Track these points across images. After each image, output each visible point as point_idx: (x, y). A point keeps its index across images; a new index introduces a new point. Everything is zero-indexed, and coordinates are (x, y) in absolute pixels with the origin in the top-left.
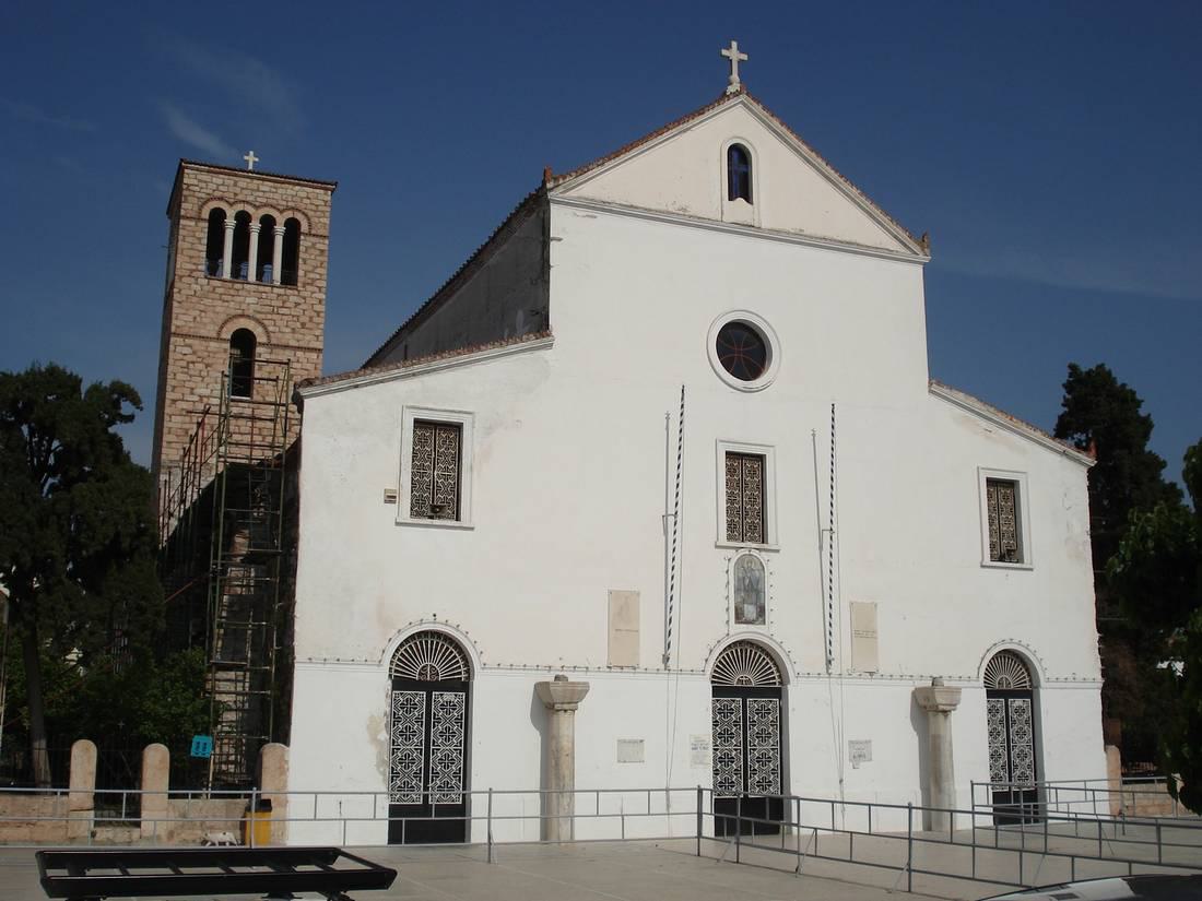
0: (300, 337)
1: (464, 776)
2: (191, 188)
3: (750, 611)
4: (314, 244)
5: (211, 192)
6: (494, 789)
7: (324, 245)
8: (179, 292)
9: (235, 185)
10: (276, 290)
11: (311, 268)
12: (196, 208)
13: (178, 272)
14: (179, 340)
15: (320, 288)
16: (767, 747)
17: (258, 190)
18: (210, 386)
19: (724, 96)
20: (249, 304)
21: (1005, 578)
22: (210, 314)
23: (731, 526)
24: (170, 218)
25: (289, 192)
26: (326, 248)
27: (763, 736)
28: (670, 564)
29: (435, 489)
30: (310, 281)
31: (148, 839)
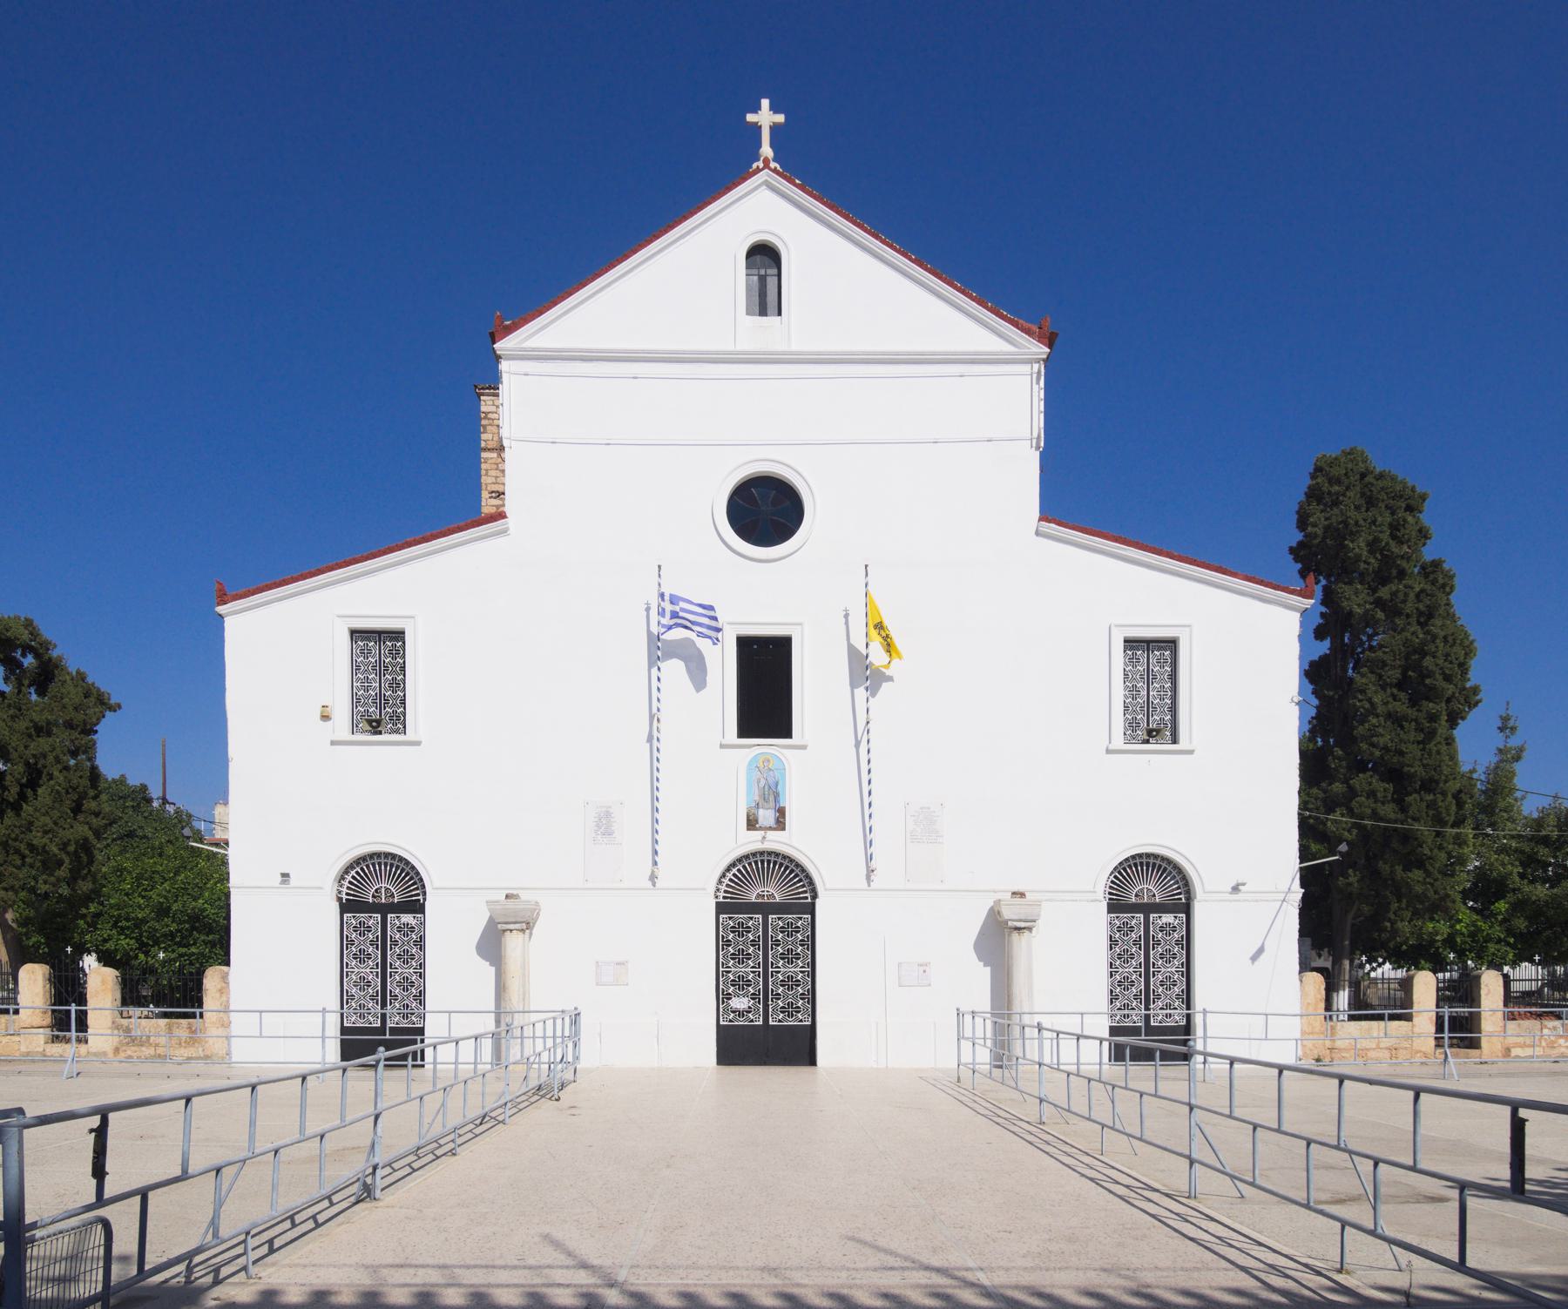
1: (1187, 999)
2: (490, 416)
3: (766, 816)
6: (327, 1009)
16: (795, 970)
23: (1132, 725)
27: (1168, 957)
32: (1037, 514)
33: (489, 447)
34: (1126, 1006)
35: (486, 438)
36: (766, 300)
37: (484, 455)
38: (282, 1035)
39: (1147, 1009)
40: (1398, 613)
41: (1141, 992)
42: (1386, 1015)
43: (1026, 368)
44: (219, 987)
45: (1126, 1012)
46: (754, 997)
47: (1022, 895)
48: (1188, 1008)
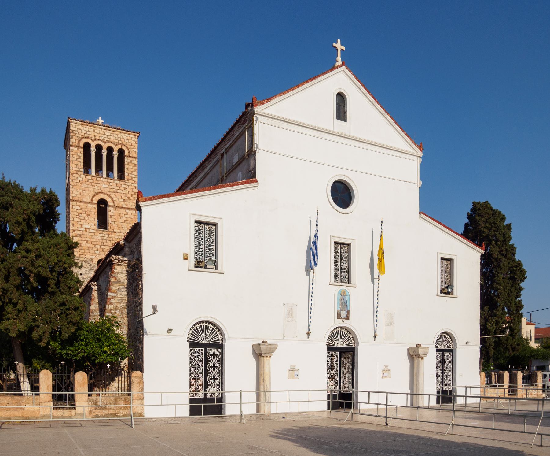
0: (128, 203)
2: (74, 132)
3: (343, 314)
4: (131, 161)
5: (83, 134)
7: (136, 161)
8: (72, 181)
9: (94, 131)
10: (115, 182)
11: (131, 172)
12: (77, 142)
13: (71, 172)
14: (74, 203)
15: (135, 181)
17: (105, 134)
18: (89, 224)
19: (333, 68)
20: (104, 188)
21: (446, 300)
22: (87, 192)
23: (336, 276)
24: (65, 149)
25: (119, 136)
26: (137, 163)
27: (214, 367)
28: (311, 290)
29: (205, 254)
30: (131, 178)
31: (80, 414)
33: (74, 145)
36: (342, 114)
37: (71, 148)
38: (167, 404)
39: (205, 391)
41: (202, 383)
48: (222, 390)
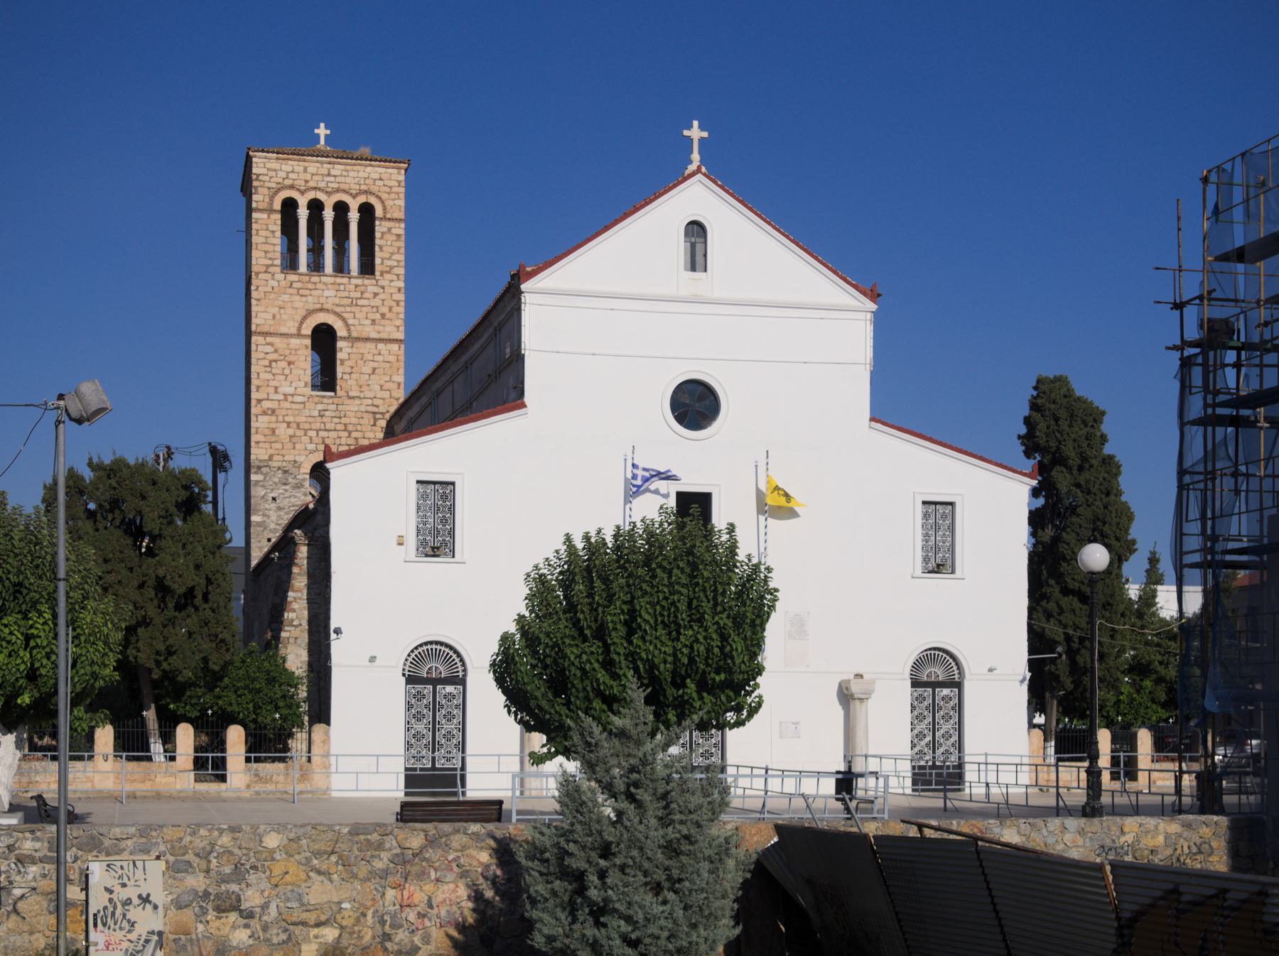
2: (260, 178)
27: (947, 718)
32: (868, 416)
34: (921, 751)
35: (346, 255)
36: (696, 260)
39: (934, 752)
40: (1089, 493)
42: (71, 754)
43: (862, 316)
44: (322, 739)
45: (449, 756)
46: (683, 745)
47: (861, 676)
